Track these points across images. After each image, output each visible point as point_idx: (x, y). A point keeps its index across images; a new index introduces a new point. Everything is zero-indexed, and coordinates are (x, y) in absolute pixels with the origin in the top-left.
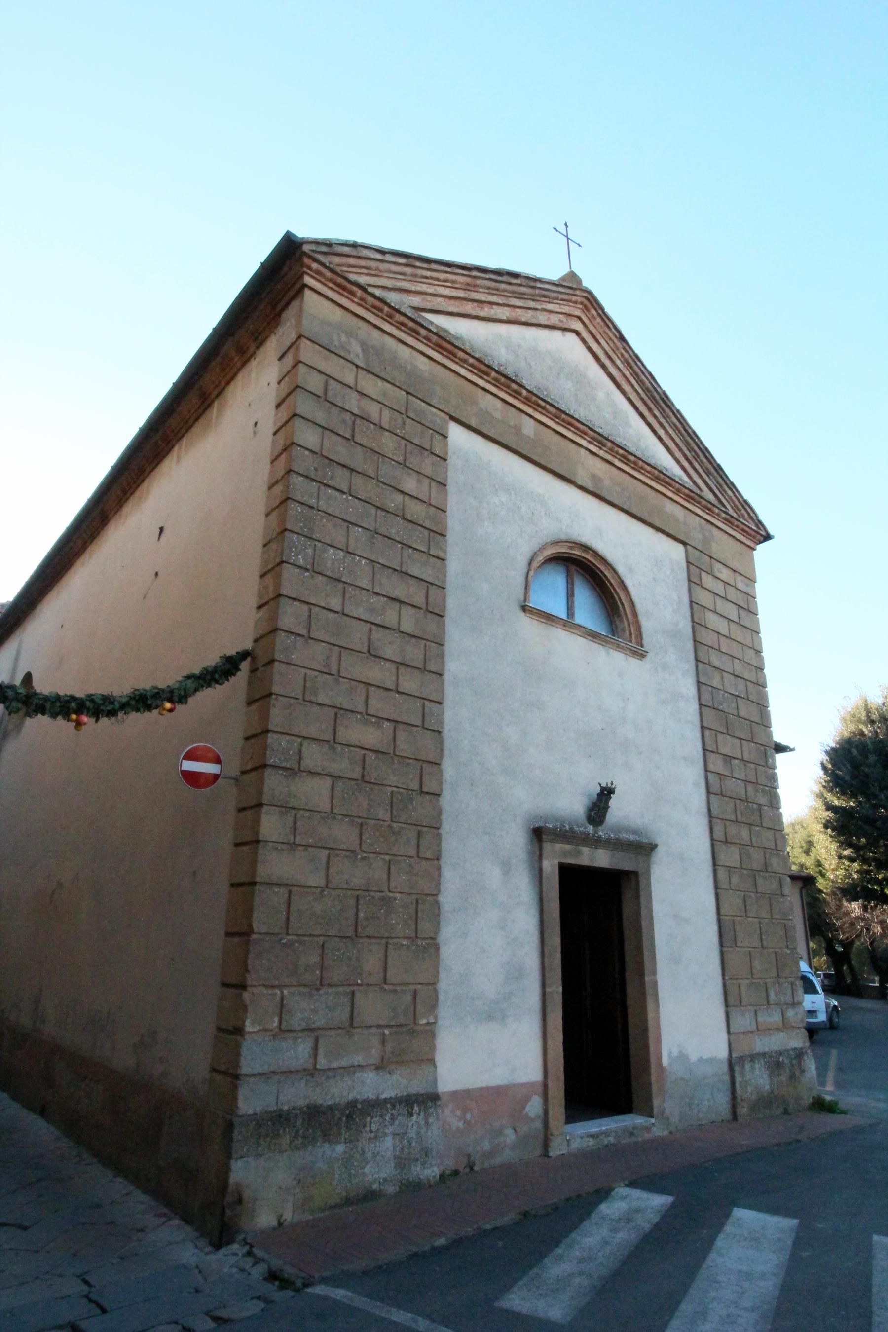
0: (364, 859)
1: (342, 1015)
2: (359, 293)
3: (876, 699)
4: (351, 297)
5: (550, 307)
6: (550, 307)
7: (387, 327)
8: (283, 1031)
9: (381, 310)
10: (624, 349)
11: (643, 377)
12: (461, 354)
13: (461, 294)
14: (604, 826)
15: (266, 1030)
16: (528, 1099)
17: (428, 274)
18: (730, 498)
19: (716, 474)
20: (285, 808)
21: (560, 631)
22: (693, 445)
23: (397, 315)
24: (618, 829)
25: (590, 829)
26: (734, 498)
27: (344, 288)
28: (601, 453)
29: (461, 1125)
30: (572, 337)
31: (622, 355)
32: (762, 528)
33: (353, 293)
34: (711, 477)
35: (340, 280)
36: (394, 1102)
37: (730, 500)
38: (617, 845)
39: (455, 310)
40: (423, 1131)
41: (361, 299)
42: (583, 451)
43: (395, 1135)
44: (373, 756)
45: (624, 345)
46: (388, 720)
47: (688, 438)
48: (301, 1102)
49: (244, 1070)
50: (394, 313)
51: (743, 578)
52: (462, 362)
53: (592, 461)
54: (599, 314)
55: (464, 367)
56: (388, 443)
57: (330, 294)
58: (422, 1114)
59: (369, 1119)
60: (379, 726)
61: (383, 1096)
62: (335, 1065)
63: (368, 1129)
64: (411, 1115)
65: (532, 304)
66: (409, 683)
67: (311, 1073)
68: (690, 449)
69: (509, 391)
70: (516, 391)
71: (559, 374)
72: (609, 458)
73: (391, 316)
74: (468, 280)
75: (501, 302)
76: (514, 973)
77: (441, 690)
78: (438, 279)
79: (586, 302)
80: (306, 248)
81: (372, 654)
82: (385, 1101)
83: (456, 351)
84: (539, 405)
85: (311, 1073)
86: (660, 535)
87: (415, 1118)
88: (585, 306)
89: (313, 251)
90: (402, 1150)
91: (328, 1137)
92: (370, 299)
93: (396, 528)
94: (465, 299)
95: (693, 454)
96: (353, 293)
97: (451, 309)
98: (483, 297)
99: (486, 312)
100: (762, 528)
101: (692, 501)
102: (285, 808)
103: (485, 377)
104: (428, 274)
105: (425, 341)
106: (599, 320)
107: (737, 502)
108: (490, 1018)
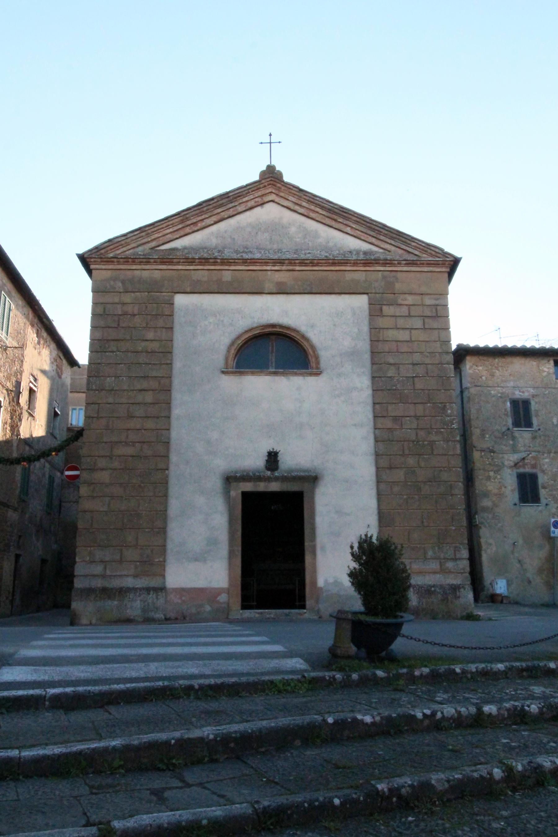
0: (126, 499)
1: (118, 557)
2: (115, 260)
3: (556, 347)
4: (113, 263)
5: (244, 200)
6: (244, 200)
7: (134, 267)
8: (92, 562)
9: (128, 262)
10: (305, 195)
11: (323, 205)
12: (175, 260)
13: (180, 226)
14: (279, 470)
15: (84, 561)
16: (219, 594)
17: (155, 229)
18: (415, 246)
19: (398, 237)
20: (90, 484)
21: (250, 377)
22: (374, 227)
23: (136, 260)
24: (290, 471)
25: (269, 473)
26: (418, 246)
27: (110, 262)
28: (284, 268)
29: (180, 601)
30: (271, 204)
31: (305, 199)
32: (449, 256)
33: (113, 262)
34: (396, 240)
35: (105, 260)
36: (141, 589)
37: (416, 248)
38: (284, 479)
39: (178, 236)
40: (155, 600)
41: (118, 262)
42: (269, 273)
43: (141, 601)
44: (131, 458)
45: (304, 193)
46: (138, 442)
47: (368, 225)
48: (99, 585)
49: (75, 574)
50: (134, 260)
51: (429, 296)
52: (178, 263)
53: (277, 275)
54: (283, 185)
55: (180, 265)
56: (138, 320)
57: (104, 267)
58: (155, 595)
59: (128, 594)
60: (133, 446)
61: (137, 587)
62: (114, 574)
63: (128, 597)
64: (149, 594)
65: (231, 205)
66: (150, 424)
67: (104, 576)
68: (374, 230)
69: (210, 264)
70: (214, 262)
71: (257, 233)
72: (291, 268)
73: (134, 262)
74: (181, 218)
75: (207, 216)
76: (212, 542)
77: (169, 424)
78: (163, 228)
79: (272, 182)
80: (86, 256)
81: (131, 417)
82: (137, 588)
83: (172, 260)
84: (231, 262)
85: (104, 576)
86: (343, 296)
87: (151, 596)
88: (273, 184)
89: (89, 255)
90: (144, 606)
91: (110, 598)
92: (121, 260)
93: (143, 358)
94: (183, 227)
95: (376, 232)
96: (113, 262)
97: (175, 237)
98: (195, 221)
99: (200, 225)
100: (449, 256)
101: (371, 265)
102: (90, 484)
103: (194, 264)
104: (155, 229)
105: (155, 264)
106: (283, 188)
107: (421, 247)
108: (196, 560)
